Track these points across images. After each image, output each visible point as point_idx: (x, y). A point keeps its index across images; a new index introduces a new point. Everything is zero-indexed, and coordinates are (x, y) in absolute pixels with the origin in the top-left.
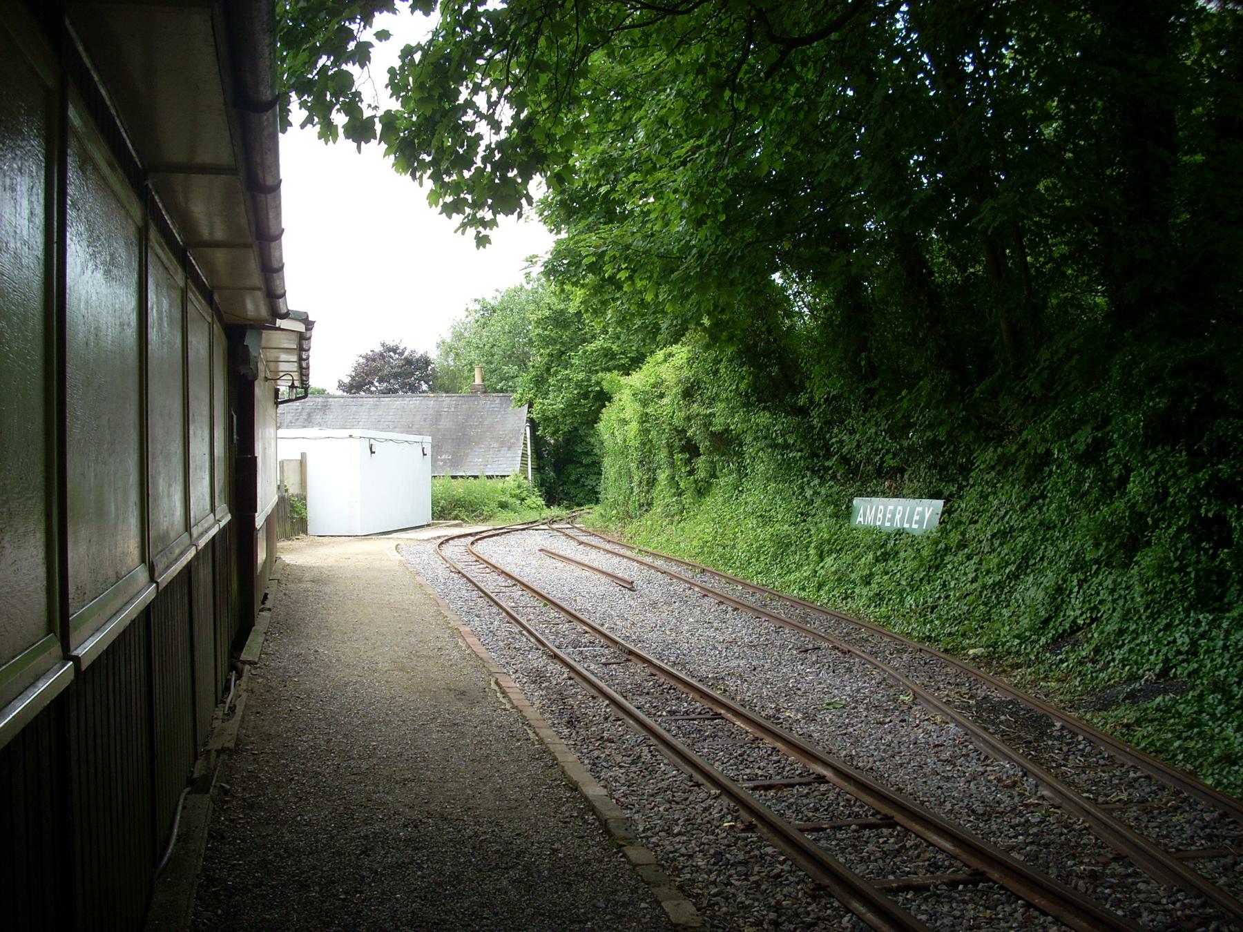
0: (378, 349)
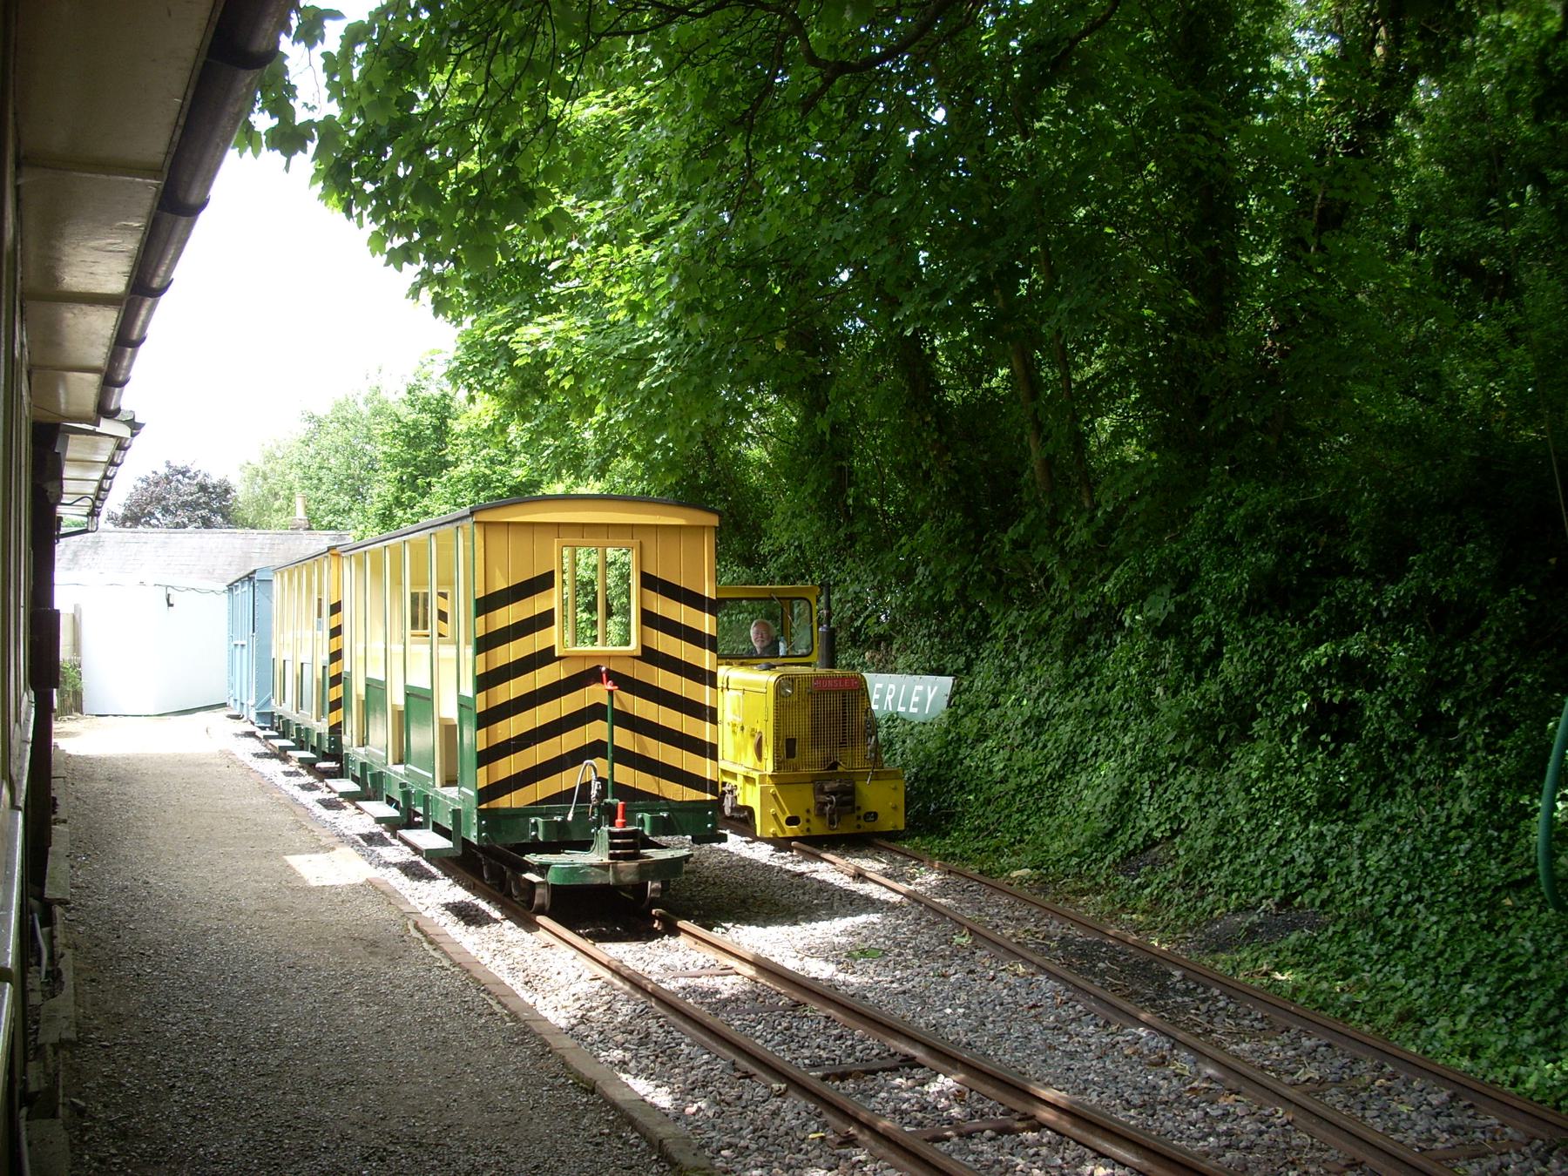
0: (163, 471)
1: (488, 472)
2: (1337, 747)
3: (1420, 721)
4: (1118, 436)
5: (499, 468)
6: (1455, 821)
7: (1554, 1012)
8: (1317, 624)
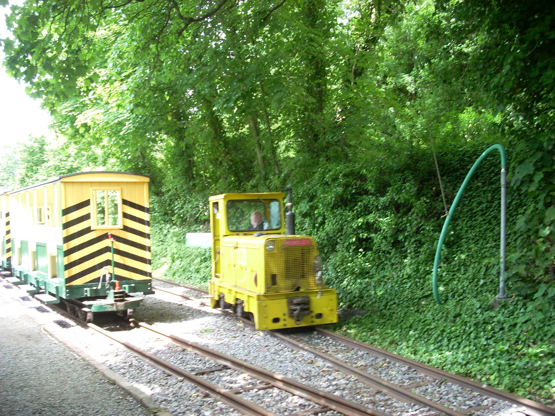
1: (59, 164)
2: (365, 253)
3: (393, 243)
4: (287, 149)
5: (63, 162)
6: (405, 277)
7: (440, 338)
8: (357, 212)
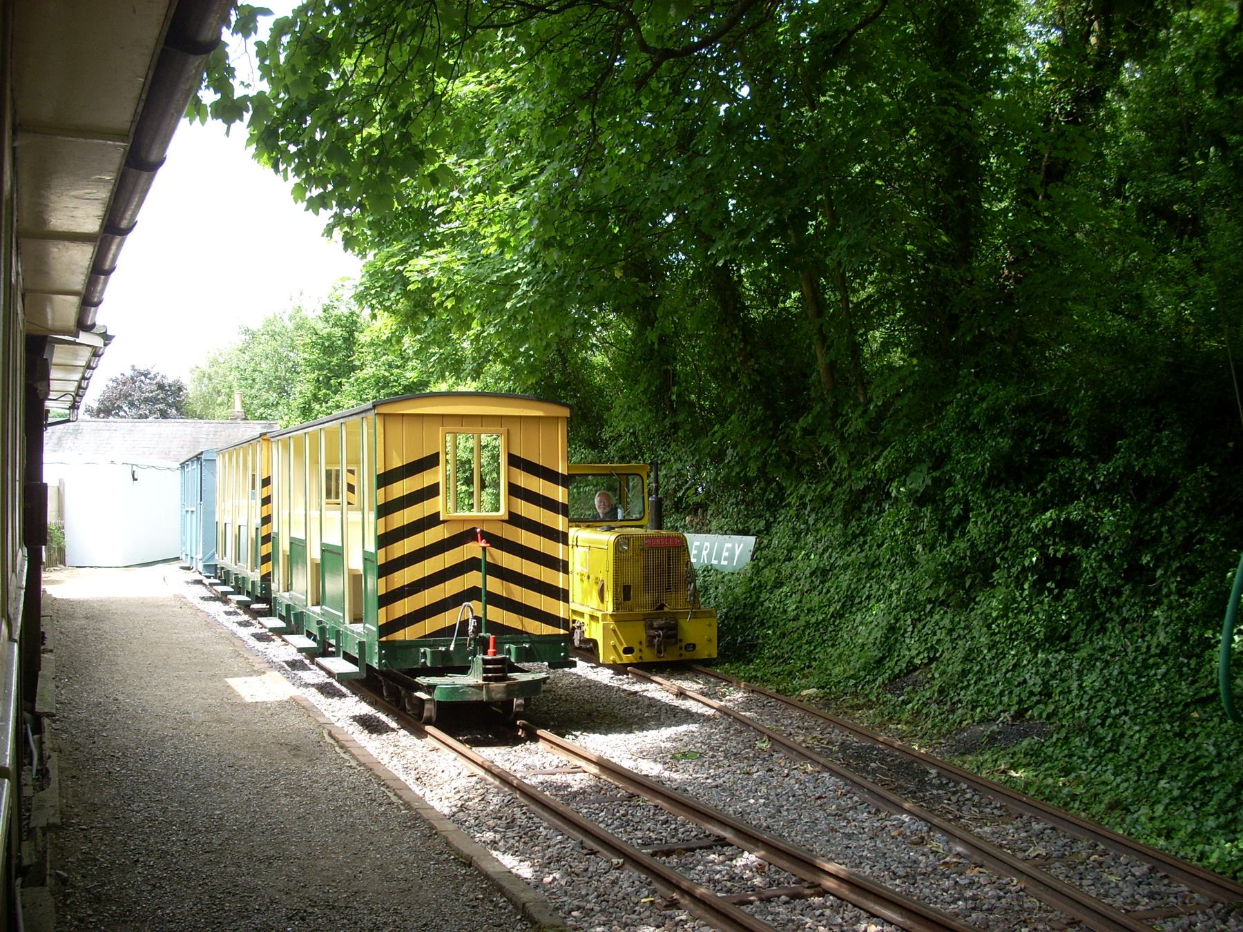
0: (129, 373)
1: (387, 374)
2: (1060, 592)
3: (1125, 571)
4: (886, 346)
5: (395, 371)
6: (1154, 651)
7: (1232, 802)
